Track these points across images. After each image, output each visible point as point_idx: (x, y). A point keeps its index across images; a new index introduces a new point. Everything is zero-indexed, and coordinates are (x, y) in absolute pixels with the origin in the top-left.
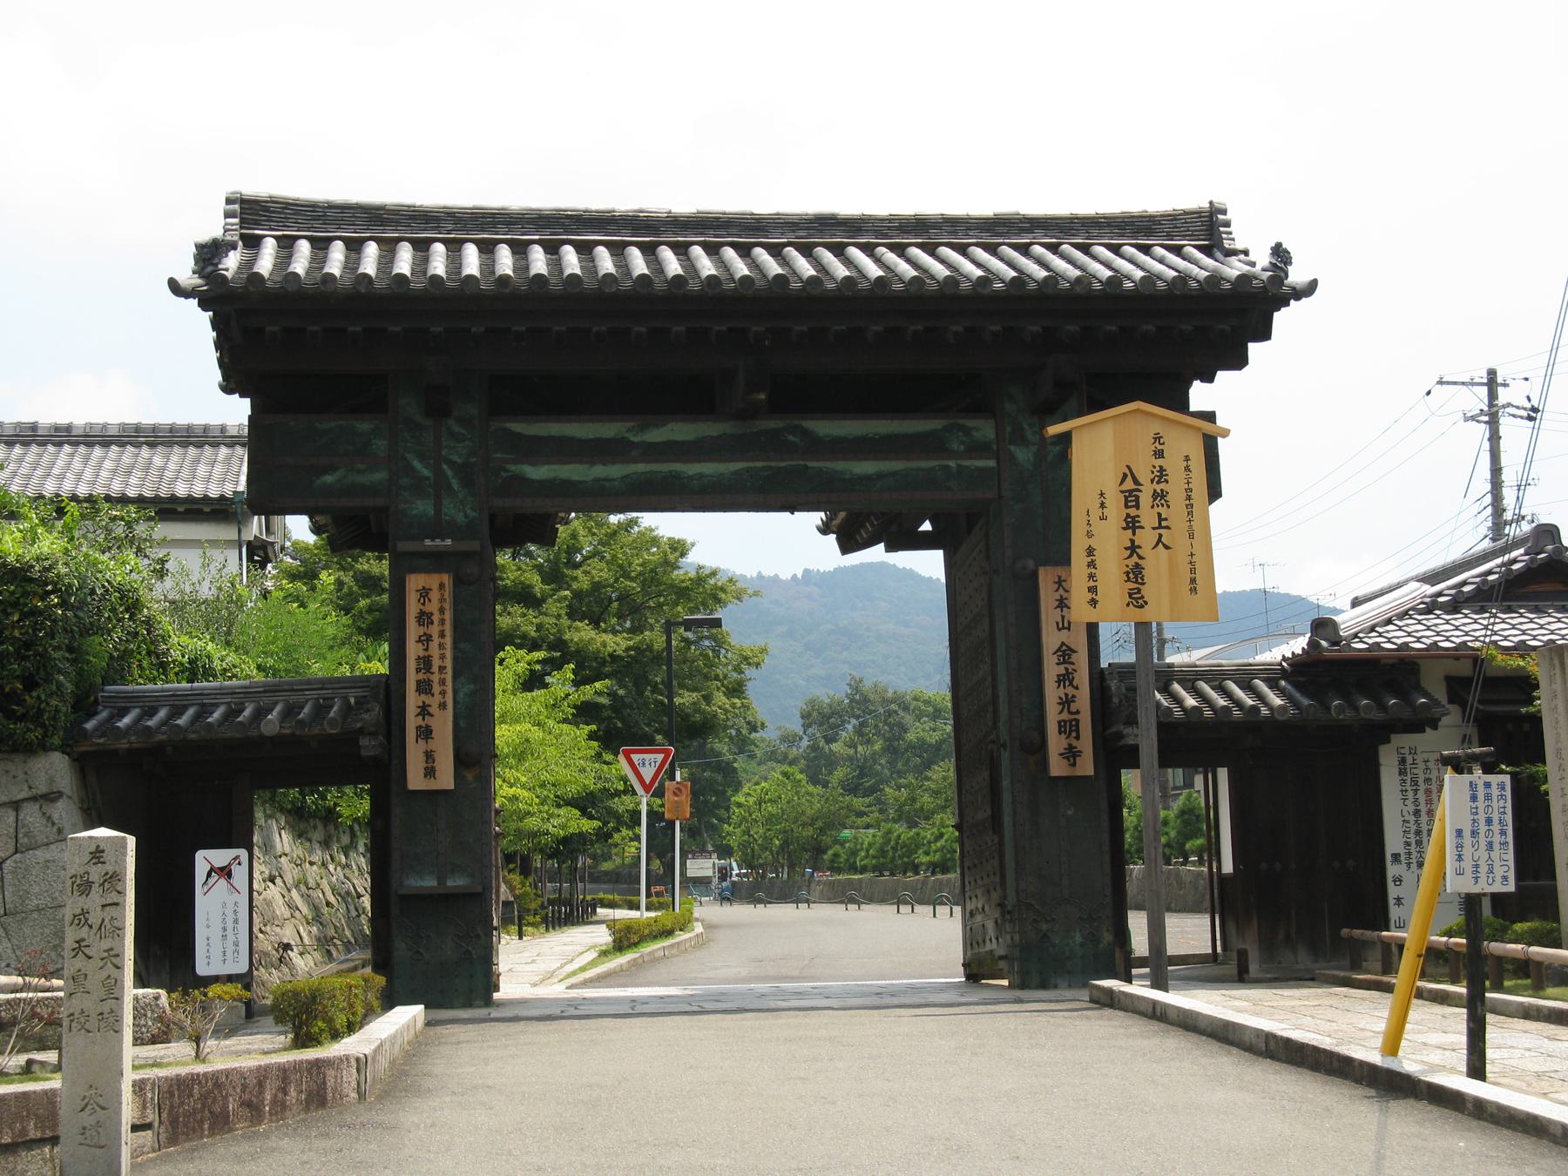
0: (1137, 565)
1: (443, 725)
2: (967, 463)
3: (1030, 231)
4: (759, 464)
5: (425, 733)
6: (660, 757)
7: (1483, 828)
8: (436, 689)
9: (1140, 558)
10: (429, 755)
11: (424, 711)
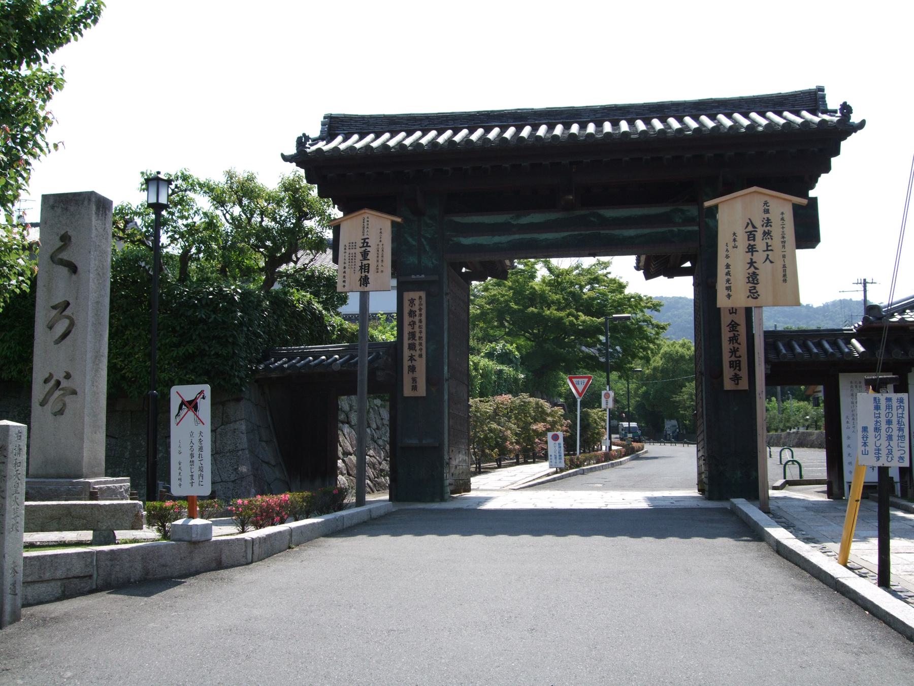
0: (754, 273)
1: (421, 365)
2: (683, 228)
3: (718, 107)
4: (576, 233)
5: (412, 369)
6: (586, 380)
7: (884, 426)
8: (418, 347)
9: (756, 268)
10: (414, 380)
11: (412, 358)
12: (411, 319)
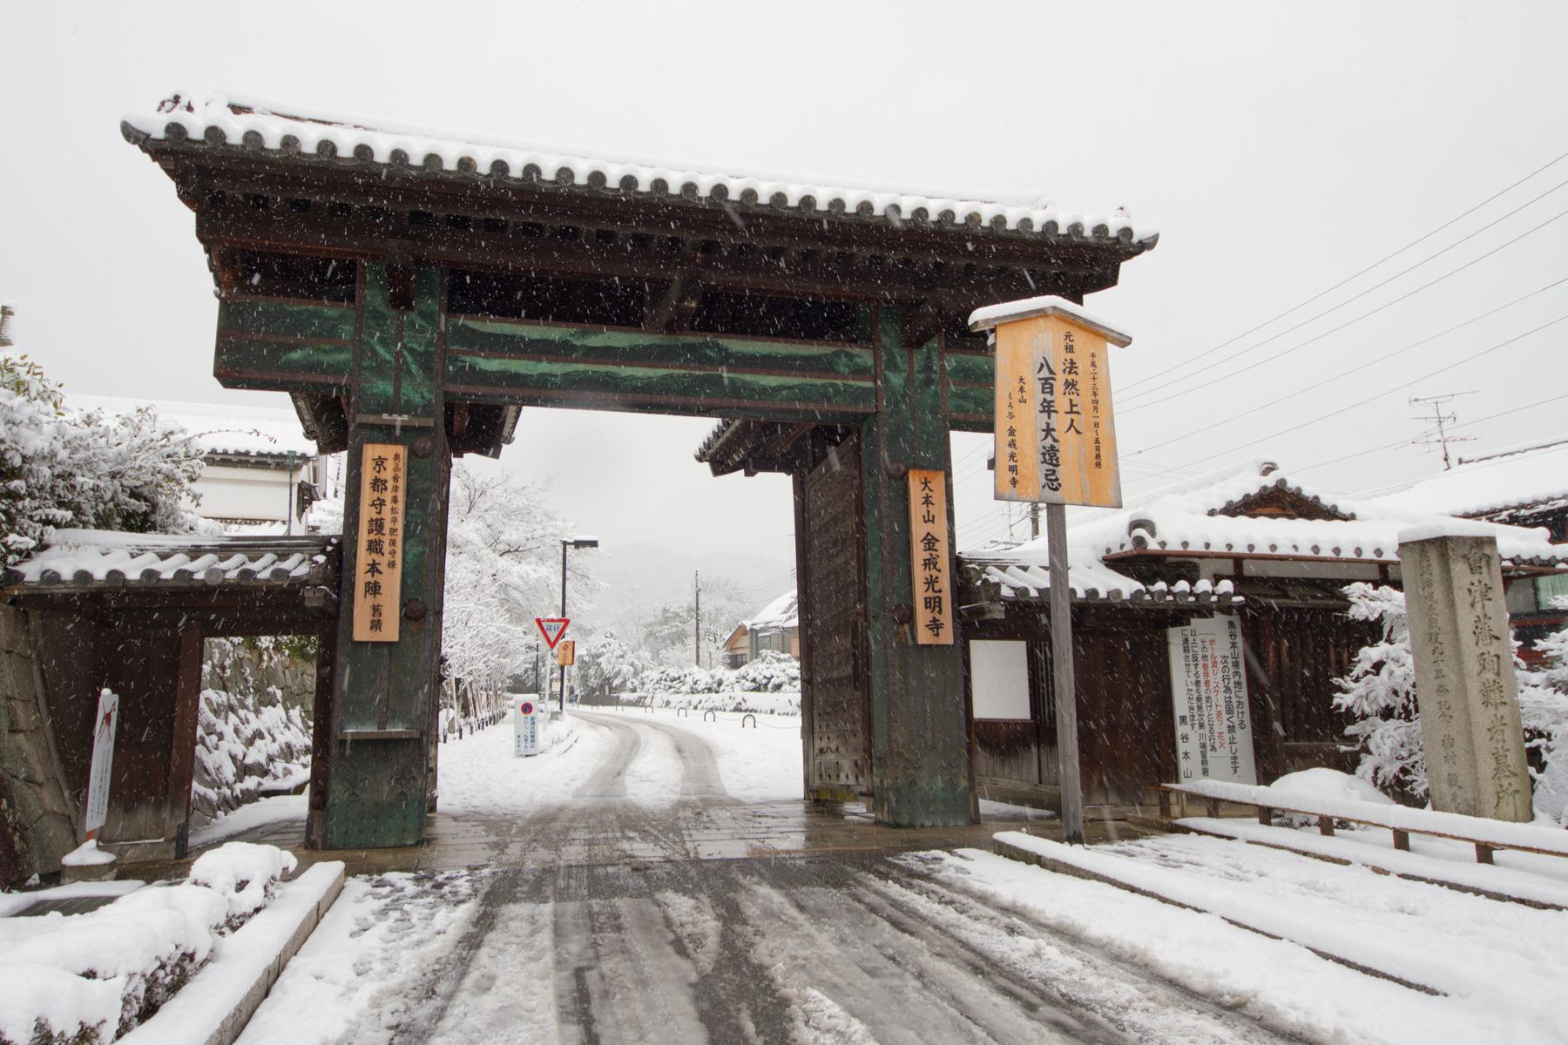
1: (391, 582)
2: (852, 382)
5: (374, 589)
8: (387, 548)
9: (1056, 441)
10: (376, 609)
11: (373, 568)
12: (376, 495)
